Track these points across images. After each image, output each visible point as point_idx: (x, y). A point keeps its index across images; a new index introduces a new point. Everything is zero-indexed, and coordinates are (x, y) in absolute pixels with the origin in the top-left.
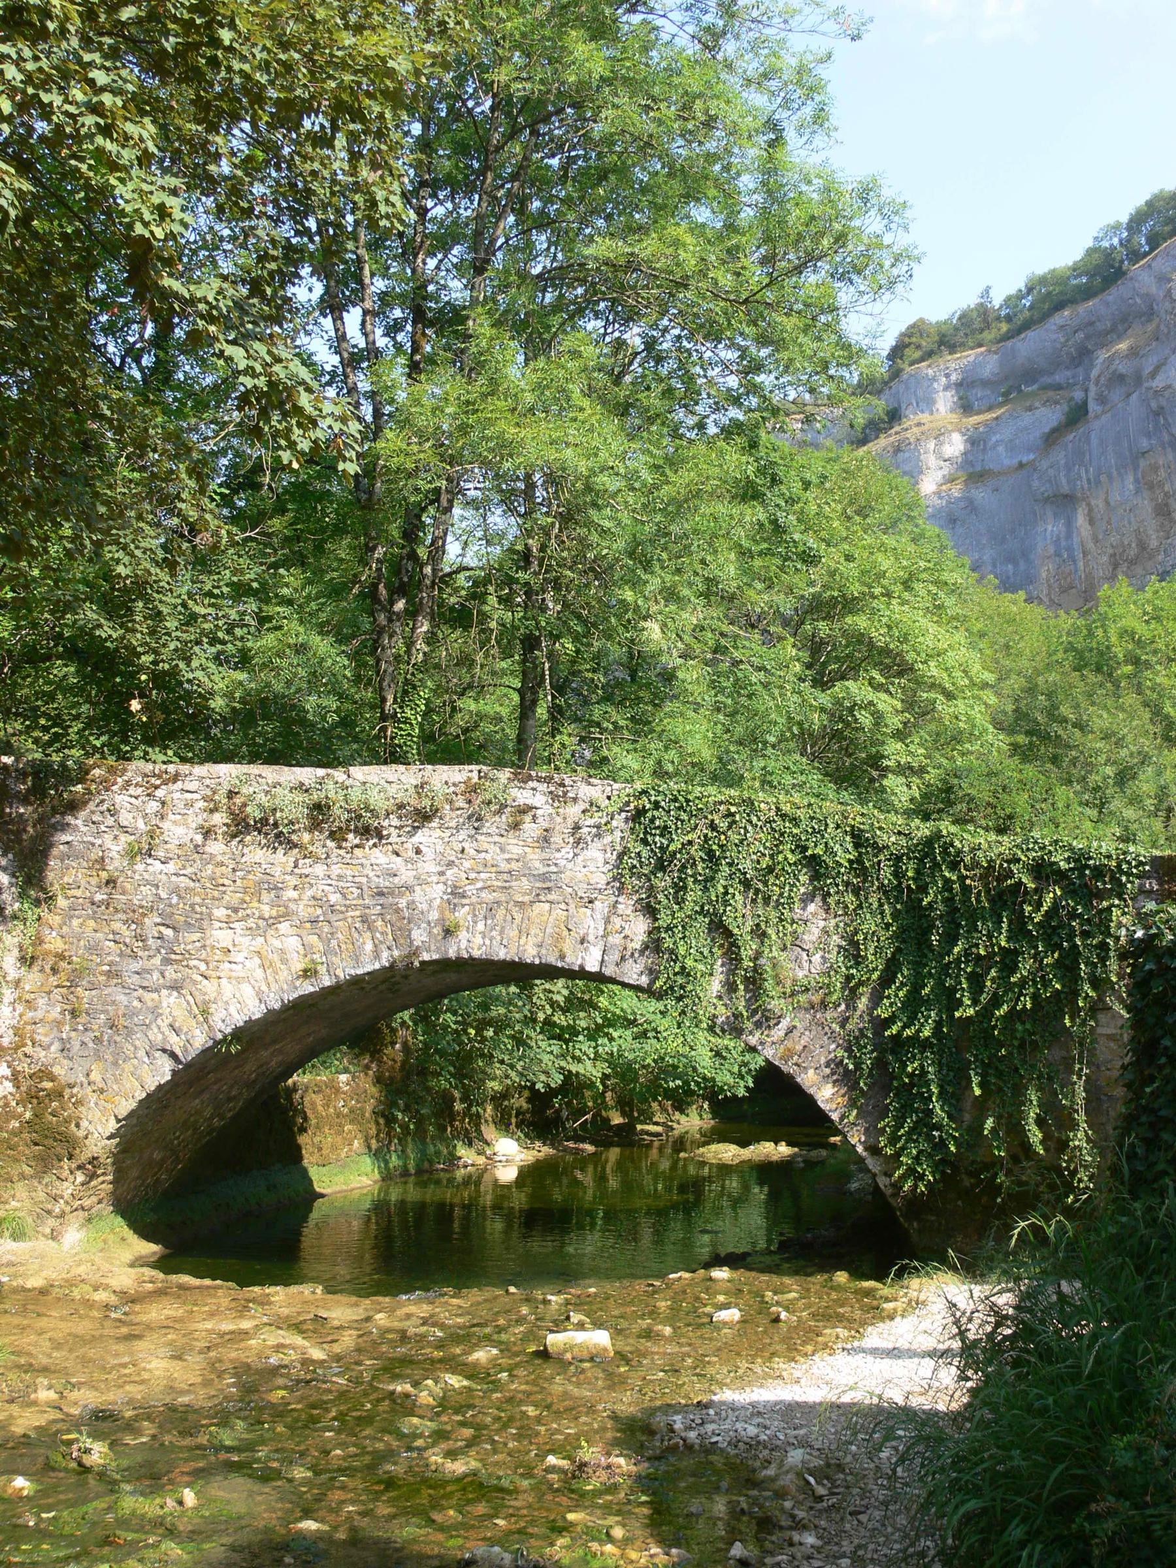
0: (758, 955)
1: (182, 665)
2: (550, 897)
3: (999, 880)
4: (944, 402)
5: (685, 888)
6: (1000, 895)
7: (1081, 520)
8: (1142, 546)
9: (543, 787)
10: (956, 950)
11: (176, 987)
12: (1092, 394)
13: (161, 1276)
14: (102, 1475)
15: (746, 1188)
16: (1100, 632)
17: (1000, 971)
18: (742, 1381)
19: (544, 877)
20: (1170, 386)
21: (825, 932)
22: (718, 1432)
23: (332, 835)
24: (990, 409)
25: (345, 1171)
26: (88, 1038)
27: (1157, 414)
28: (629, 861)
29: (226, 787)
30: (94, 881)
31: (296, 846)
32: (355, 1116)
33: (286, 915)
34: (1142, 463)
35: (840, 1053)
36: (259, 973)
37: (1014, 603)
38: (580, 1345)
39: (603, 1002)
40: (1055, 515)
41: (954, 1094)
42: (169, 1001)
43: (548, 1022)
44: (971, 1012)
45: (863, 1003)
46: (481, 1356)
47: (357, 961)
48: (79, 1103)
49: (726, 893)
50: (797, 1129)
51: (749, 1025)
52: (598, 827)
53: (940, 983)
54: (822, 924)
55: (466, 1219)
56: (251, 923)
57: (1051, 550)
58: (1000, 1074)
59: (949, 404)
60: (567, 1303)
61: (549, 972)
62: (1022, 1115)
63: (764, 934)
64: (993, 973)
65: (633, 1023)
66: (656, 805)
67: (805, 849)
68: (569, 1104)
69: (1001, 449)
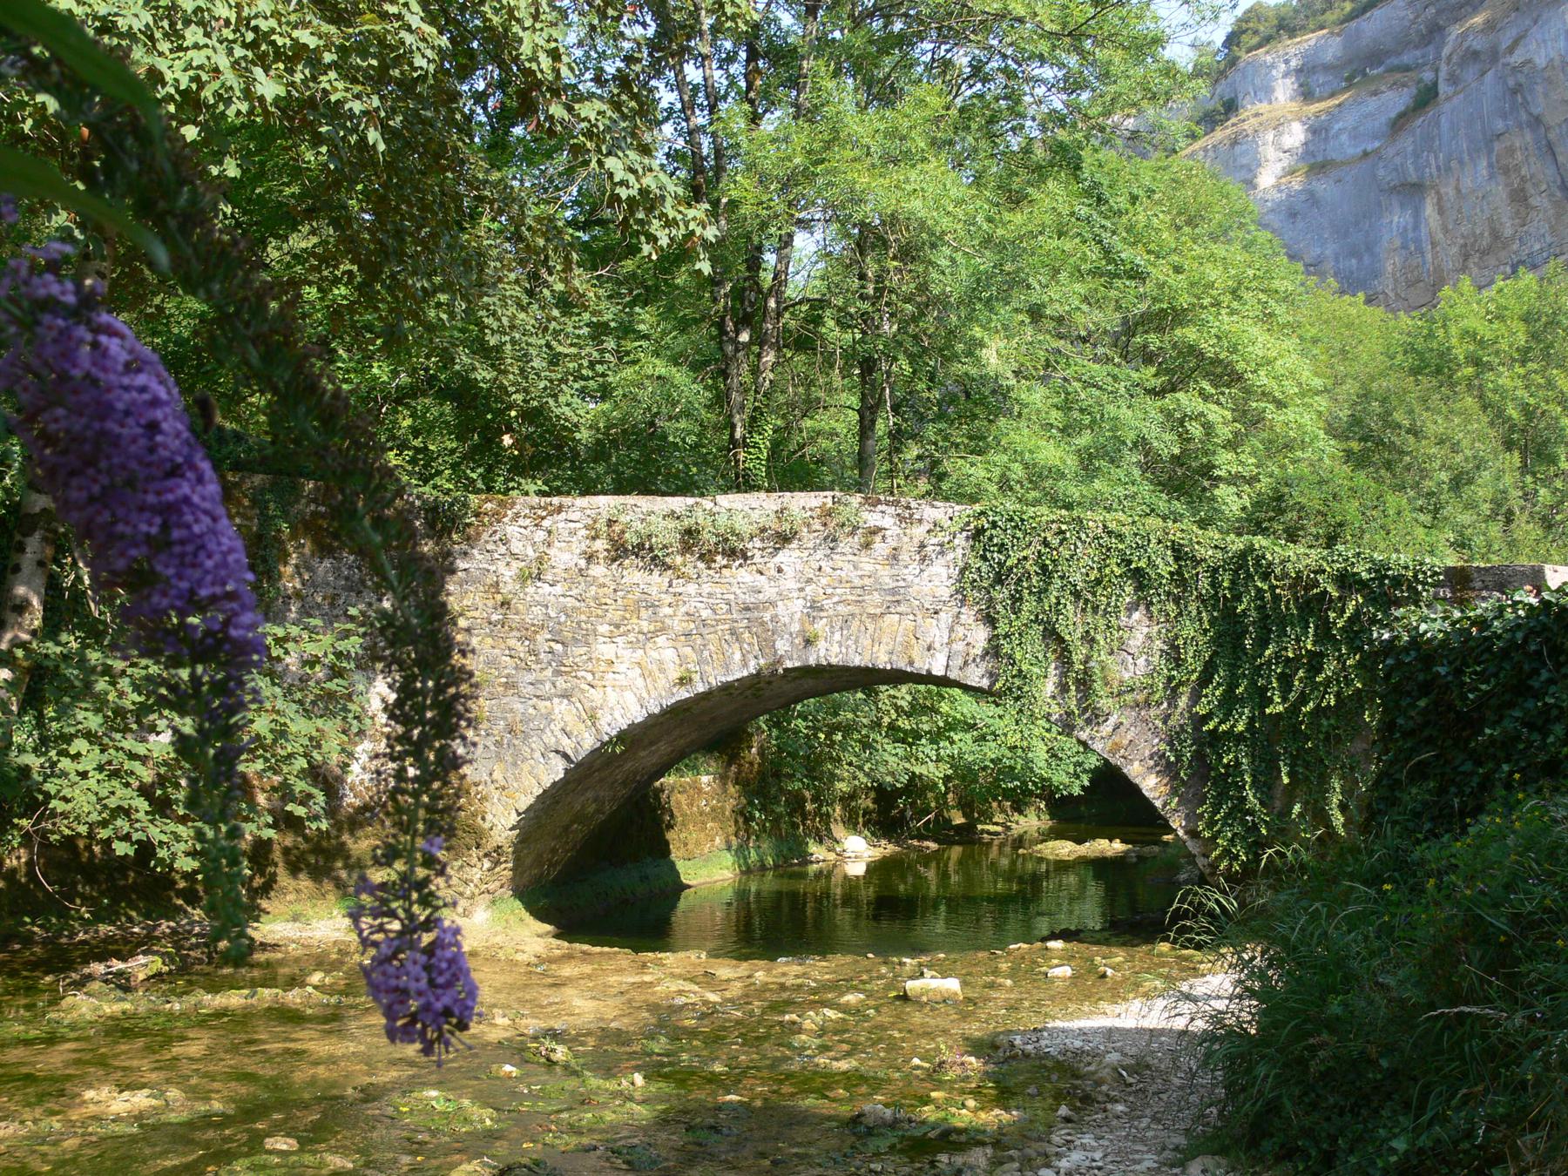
0: (1088, 658)
1: (551, 402)
2: (899, 609)
3: (1306, 589)
4: (1284, 90)
5: (1021, 599)
6: (1308, 602)
7: (1429, 210)
8: (1496, 235)
9: (891, 510)
10: (1267, 653)
11: (566, 695)
12: (1443, 74)
13: (566, 944)
14: (566, 1067)
15: (1083, 886)
16: (1441, 333)
17: (1307, 671)
18: (1071, 1016)
19: (894, 592)
20: (1529, 61)
21: (1149, 637)
22: (1049, 1045)
23: (702, 557)
24: (1332, 95)
25: (708, 865)
26: (490, 742)
27: (1514, 92)
28: (969, 576)
29: (605, 516)
30: (490, 603)
31: (670, 568)
32: (716, 814)
33: (663, 630)
34: (1497, 146)
35: (1163, 746)
36: (640, 682)
37: (1354, 306)
38: (934, 990)
39: (944, 707)
40: (1402, 205)
41: (1265, 784)
42: (561, 707)
43: (892, 727)
44: (1280, 708)
45: (1183, 702)
46: (851, 998)
47: (727, 668)
48: (483, 799)
49: (1058, 603)
50: (1131, 829)
51: (1080, 722)
52: (942, 545)
53: (1253, 683)
54: (1146, 630)
55: (819, 911)
56: (631, 637)
57: (1398, 243)
58: (1307, 765)
59: (1289, 92)
60: (920, 965)
61: (897, 677)
62: (1326, 801)
63: (1093, 640)
64: (1301, 673)
65: (973, 727)
66: (994, 525)
67: (1129, 562)
68: (913, 804)
69: (1344, 137)
